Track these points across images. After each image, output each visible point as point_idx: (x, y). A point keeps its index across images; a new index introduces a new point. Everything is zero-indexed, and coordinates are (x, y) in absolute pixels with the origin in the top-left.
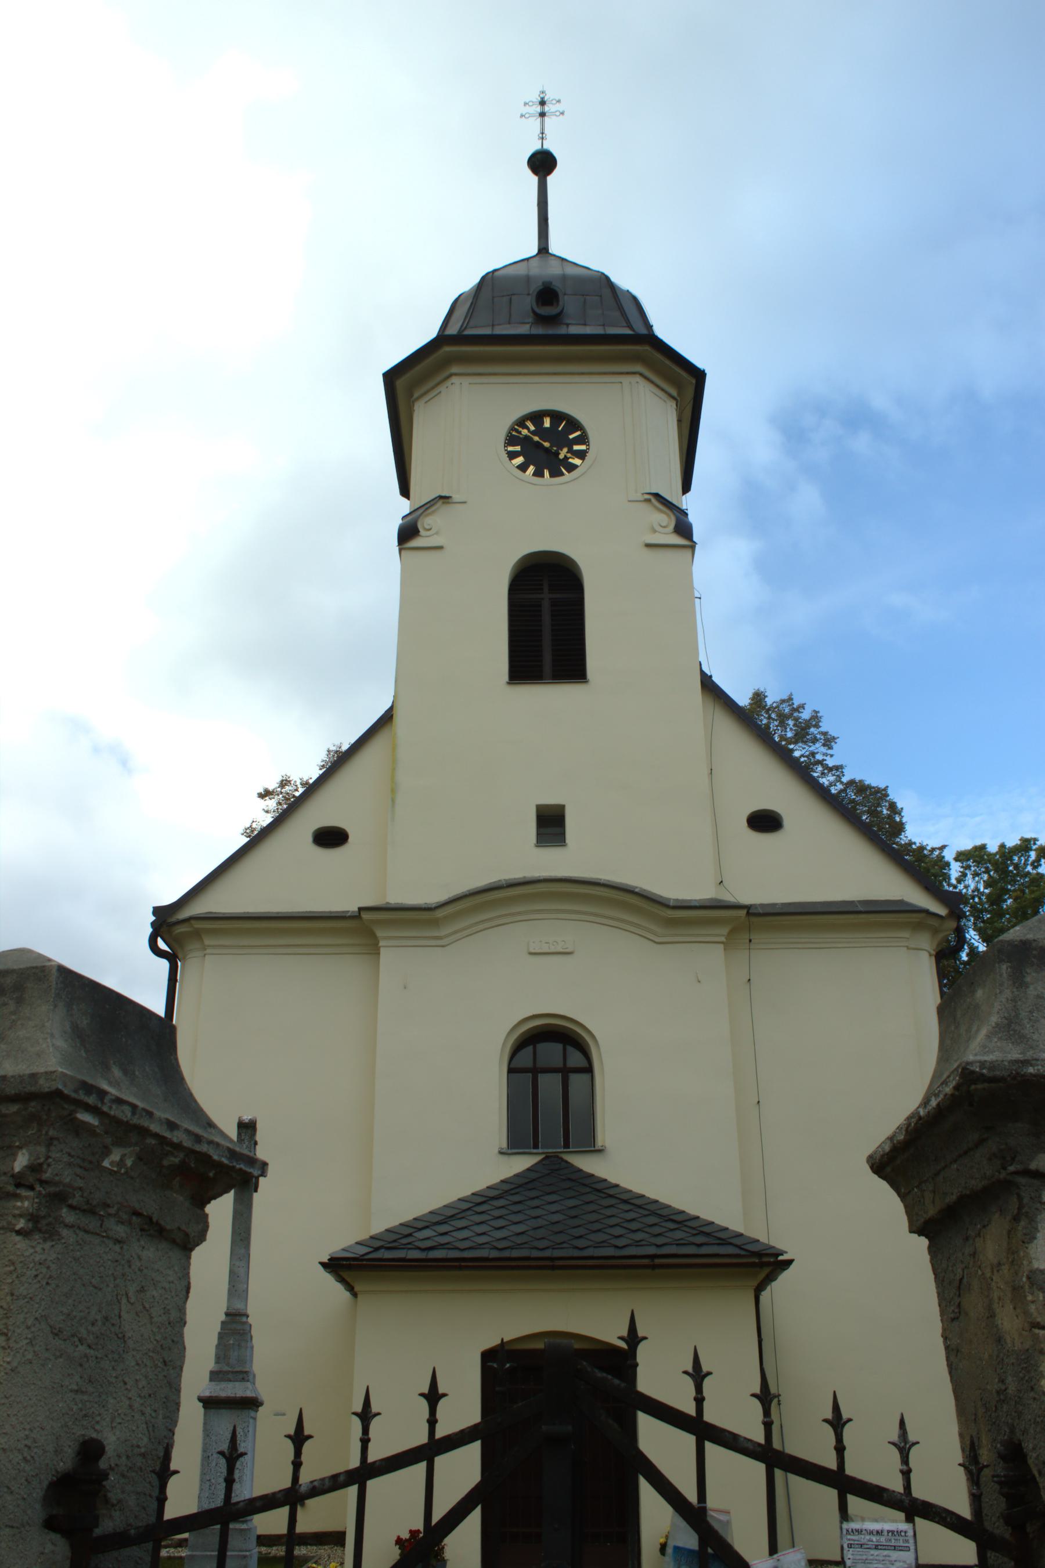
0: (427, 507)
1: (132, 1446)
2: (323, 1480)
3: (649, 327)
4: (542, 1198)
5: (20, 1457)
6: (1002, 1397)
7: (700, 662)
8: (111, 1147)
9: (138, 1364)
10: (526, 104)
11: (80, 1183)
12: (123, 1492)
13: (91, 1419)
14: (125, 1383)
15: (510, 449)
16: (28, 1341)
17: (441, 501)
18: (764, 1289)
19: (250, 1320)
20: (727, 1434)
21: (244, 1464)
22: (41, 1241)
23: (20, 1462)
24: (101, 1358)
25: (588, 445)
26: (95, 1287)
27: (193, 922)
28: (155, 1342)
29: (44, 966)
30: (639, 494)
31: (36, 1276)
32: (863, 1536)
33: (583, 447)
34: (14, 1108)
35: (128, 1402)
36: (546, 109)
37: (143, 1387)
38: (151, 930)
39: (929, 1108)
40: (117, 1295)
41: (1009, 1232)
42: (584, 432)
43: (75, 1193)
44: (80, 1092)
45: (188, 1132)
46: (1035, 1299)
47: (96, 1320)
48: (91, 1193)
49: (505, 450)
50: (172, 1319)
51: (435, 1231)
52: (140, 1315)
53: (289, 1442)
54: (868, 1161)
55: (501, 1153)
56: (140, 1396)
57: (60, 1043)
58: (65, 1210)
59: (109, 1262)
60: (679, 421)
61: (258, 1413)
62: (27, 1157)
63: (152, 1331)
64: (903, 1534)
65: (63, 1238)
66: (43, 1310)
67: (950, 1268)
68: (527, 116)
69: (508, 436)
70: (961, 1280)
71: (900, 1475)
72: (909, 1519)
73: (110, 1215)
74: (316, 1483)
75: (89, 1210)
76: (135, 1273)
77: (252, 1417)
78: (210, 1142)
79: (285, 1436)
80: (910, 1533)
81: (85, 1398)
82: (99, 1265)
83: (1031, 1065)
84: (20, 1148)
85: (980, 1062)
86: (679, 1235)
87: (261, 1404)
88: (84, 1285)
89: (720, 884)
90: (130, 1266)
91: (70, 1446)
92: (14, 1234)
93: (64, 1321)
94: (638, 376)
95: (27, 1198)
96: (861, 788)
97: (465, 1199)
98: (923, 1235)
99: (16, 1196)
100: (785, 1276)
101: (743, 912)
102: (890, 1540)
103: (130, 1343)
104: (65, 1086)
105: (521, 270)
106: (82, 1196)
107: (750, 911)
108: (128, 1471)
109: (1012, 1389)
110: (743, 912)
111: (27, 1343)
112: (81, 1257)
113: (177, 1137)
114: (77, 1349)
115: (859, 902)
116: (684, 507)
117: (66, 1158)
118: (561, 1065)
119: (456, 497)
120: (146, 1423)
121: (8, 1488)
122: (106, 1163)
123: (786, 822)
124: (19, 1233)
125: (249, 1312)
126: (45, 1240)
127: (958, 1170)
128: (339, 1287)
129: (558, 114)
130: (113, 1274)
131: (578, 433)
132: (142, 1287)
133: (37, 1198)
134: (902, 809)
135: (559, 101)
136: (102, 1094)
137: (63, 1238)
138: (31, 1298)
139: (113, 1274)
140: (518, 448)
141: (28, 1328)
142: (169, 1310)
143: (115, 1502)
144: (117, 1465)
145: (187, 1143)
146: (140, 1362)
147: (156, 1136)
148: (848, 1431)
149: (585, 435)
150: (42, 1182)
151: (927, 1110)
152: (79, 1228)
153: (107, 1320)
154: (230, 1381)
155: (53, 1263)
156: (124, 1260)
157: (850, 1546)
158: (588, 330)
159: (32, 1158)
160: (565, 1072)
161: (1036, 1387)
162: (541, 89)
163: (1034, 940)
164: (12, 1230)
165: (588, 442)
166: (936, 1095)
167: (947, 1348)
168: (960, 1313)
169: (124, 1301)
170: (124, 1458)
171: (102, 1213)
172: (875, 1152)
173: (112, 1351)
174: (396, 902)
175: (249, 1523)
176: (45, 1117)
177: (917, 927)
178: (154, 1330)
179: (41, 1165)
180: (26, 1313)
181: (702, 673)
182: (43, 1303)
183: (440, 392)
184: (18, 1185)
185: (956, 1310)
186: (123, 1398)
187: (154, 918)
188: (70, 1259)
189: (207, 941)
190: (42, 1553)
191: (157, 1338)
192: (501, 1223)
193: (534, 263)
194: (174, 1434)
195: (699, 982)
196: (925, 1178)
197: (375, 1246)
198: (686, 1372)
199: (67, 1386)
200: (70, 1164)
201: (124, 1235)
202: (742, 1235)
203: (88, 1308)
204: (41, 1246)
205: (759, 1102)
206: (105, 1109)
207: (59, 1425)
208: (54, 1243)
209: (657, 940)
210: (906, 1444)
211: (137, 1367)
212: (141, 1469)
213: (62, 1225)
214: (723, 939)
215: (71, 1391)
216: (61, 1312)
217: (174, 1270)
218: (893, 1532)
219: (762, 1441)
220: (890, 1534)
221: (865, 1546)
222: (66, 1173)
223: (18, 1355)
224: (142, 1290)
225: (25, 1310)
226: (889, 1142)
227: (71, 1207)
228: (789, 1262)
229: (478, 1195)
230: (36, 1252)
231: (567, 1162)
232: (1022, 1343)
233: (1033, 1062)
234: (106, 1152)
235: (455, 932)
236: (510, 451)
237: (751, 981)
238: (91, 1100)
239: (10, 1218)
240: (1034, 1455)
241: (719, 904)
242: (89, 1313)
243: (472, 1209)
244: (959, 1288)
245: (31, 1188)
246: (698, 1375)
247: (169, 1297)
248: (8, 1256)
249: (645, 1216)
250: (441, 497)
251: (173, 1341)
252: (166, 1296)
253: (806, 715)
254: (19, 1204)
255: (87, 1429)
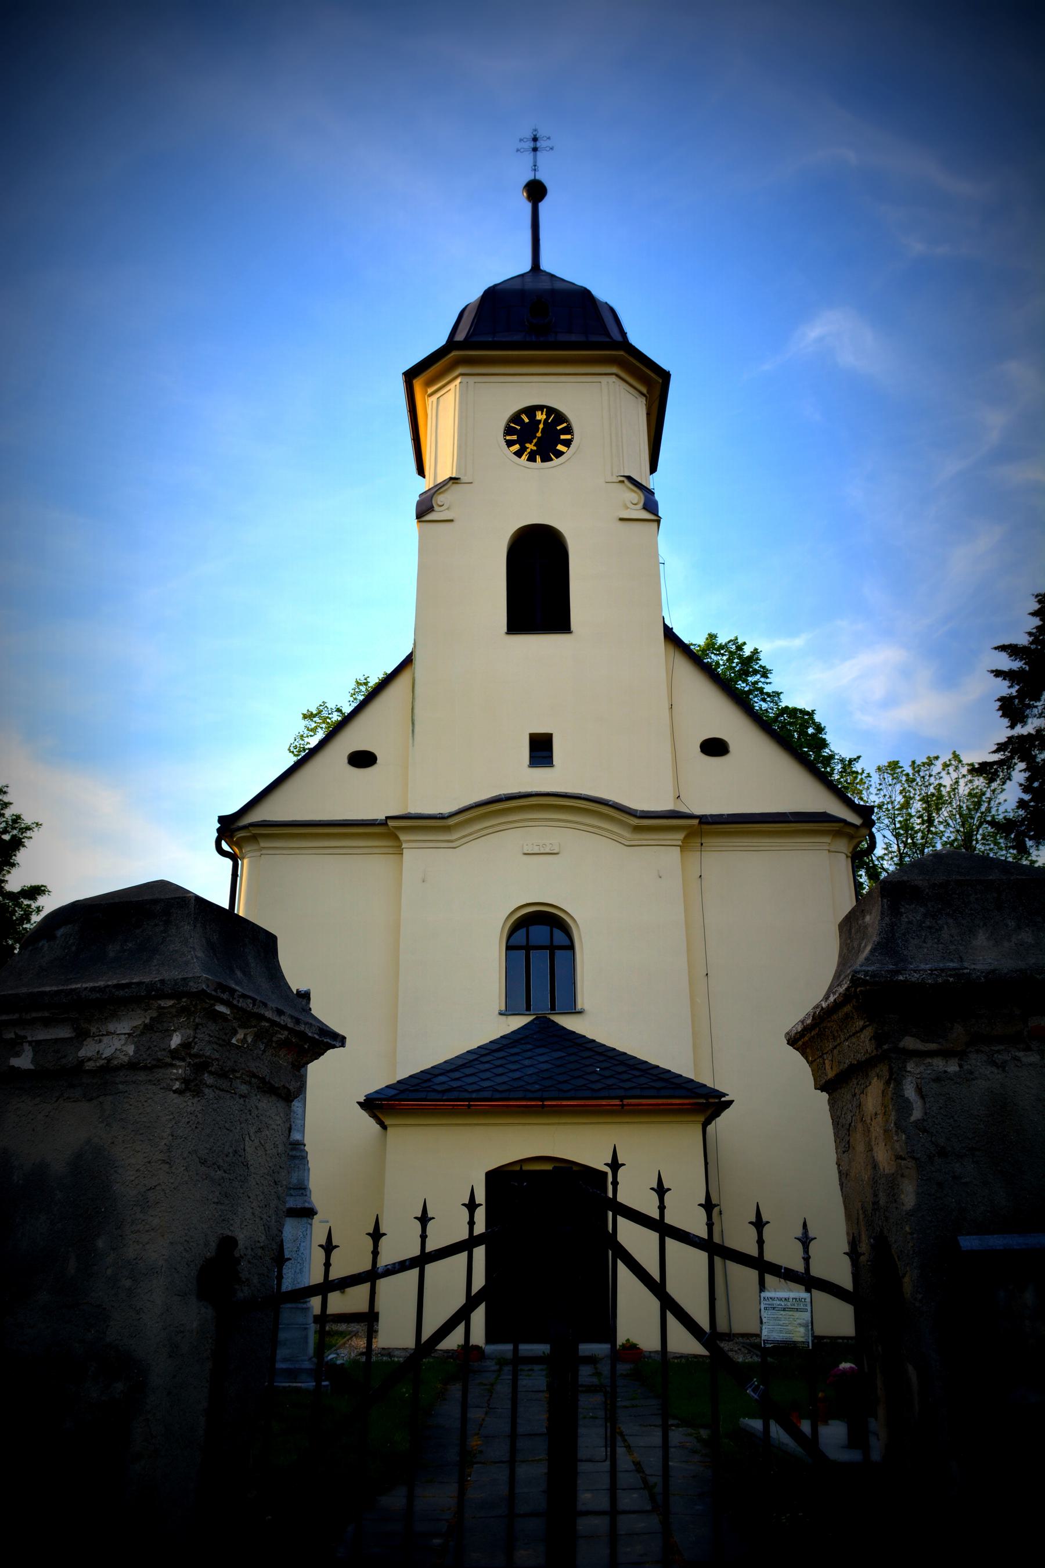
0: (439, 488)
1: (255, 1241)
2: (394, 1264)
3: (624, 334)
4: (533, 1050)
5: (182, 1248)
6: (876, 1207)
7: (663, 617)
8: (238, 1029)
9: (257, 1184)
10: (521, 140)
11: (217, 1055)
12: (250, 1273)
13: (227, 1223)
14: (249, 1198)
15: (508, 438)
16: (184, 1168)
17: (452, 481)
18: (710, 1123)
19: (306, 1148)
20: (681, 1232)
21: (304, 1259)
22: (191, 1097)
23: (183, 1251)
24: (233, 1180)
25: (573, 435)
26: (228, 1130)
27: (250, 828)
28: (268, 1168)
29: (185, 897)
30: (615, 477)
31: (188, 1122)
32: (775, 1302)
33: (568, 437)
34: (170, 1003)
35: (251, 1211)
36: (538, 144)
37: (261, 1200)
38: (216, 835)
39: (829, 1002)
40: (242, 1135)
41: (883, 1092)
42: (569, 424)
43: (213, 1062)
44: (218, 990)
45: (292, 1017)
46: (899, 1139)
47: (229, 1153)
48: (224, 1062)
49: (505, 439)
50: (279, 1152)
51: (448, 1077)
52: (258, 1149)
53: (369, 1238)
54: (785, 1037)
55: (501, 1014)
56: (259, 1207)
57: (200, 954)
58: (206, 1075)
59: (237, 1112)
60: (648, 414)
61: (314, 1220)
62: (180, 1037)
63: (266, 1160)
64: (803, 1300)
65: (205, 1095)
66: (194, 1146)
67: (843, 1116)
68: (522, 150)
69: (506, 427)
70: (850, 1125)
71: (802, 1260)
72: (808, 1290)
73: (237, 1078)
74: (388, 1267)
75: (223, 1074)
76: (254, 1118)
77: (309, 1224)
78: (306, 1023)
79: (367, 1234)
80: (808, 1300)
81: (223, 1207)
82: (230, 1113)
83: (901, 974)
84: (175, 1031)
85: (864, 971)
86: (643, 1080)
87: (316, 1213)
88: (220, 1128)
89: (678, 798)
90: (250, 1114)
91: (214, 1241)
92: (171, 1093)
93: (208, 1153)
94: (614, 376)
95: (180, 1067)
96: (793, 712)
97: (473, 1051)
98: (825, 1092)
99: (172, 1066)
100: (726, 1114)
101: (696, 822)
102: (794, 1305)
103: (252, 1169)
104: (208, 986)
105: (518, 286)
106: (218, 1065)
107: (702, 821)
108: (252, 1259)
109: (882, 1202)
110: (696, 822)
111: (184, 1170)
112: (218, 1108)
113: (284, 1021)
114: (217, 1174)
115: (791, 813)
116: (651, 487)
117: (207, 1038)
118: (548, 943)
119: (464, 479)
120: (264, 1225)
121: (175, 1269)
122: (234, 1041)
123: (732, 748)
124: (175, 1092)
125: (306, 1142)
126: (194, 1097)
127: (849, 1046)
128: (372, 1121)
129: (548, 149)
130: (239, 1120)
131: (565, 425)
132: (259, 1129)
133: (188, 1067)
134: (825, 727)
135: (549, 138)
136: (232, 991)
137: (205, 1095)
138: (185, 1138)
139: (239, 1120)
140: (515, 437)
141: (184, 1159)
142: (277, 1145)
143: (244, 1280)
144: (245, 1255)
145: (290, 1025)
146: (259, 1183)
147: (268, 1020)
148: (767, 1231)
149: (571, 427)
150: (191, 1056)
151: (827, 1004)
152: (216, 1088)
153: (236, 1153)
154: (292, 1195)
155: (200, 1113)
156: (246, 1109)
157: (766, 1309)
158: (574, 338)
159: (185, 1038)
160: (552, 948)
161: (898, 1199)
162: (534, 128)
163: (908, 881)
164: (171, 1090)
165: (573, 432)
166: (834, 993)
167: (840, 1172)
168: (849, 1146)
169: (247, 1139)
170: (250, 1250)
171: (231, 1076)
172: (791, 1031)
173: (240, 1175)
174: (416, 812)
175: (308, 1304)
176: (193, 1009)
177: (837, 834)
178: (268, 1160)
179: (190, 1043)
180: (183, 1149)
181: (665, 626)
182: (194, 1141)
183: (450, 390)
184: (173, 1058)
185: (847, 1146)
186: (248, 1207)
187: (219, 825)
188: (211, 1110)
189: (263, 844)
190: (199, 1313)
191: (270, 1165)
192: (500, 1070)
193: (528, 279)
194: (282, 1233)
195: (660, 877)
196: (826, 1051)
197: (401, 1089)
198: (652, 1189)
199: (211, 1200)
200: (209, 1042)
201: (246, 1092)
202: (692, 1080)
203: (224, 1144)
204: (191, 1101)
205: (707, 974)
206: (235, 1002)
207: (207, 1226)
208: (200, 1099)
209: (626, 844)
210: (807, 1240)
211: (257, 1186)
212: (261, 1257)
213: (205, 1086)
214: (680, 843)
215: (214, 1203)
216: (206, 1147)
217: (280, 1117)
218: (796, 1299)
219: (705, 1236)
220: (794, 1300)
221: (777, 1309)
222: (207, 1049)
223: (178, 1178)
224: (259, 1130)
225: (182, 1147)
226: (800, 1024)
227: (211, 1073)
228: (731, 1102)
229: (483, 1048)
230: (188, 1105)
231: (553, 1021)
232: (889, 1169)
233: (903, 972)
234: (235, 1033)
235: (464, 837)
236: (508, 440)
237: (702, 877)
238: (225, 996)
239: (169, 1081)
240: (896, 1247)
241: (676, 815)
242: (224, 1148)
243: (491, 1070)
244: (849, 1130)
245: (183, 1060)
246: (661, 1190)
247: (277, 1136)
248: (168, 1108)
249: (616, 1065)
250: (451, 479)
251: (280, 1167)
252: (275, 1135)
253: (747, 652)
254: (175, 1071)
255: (225, 1229)
